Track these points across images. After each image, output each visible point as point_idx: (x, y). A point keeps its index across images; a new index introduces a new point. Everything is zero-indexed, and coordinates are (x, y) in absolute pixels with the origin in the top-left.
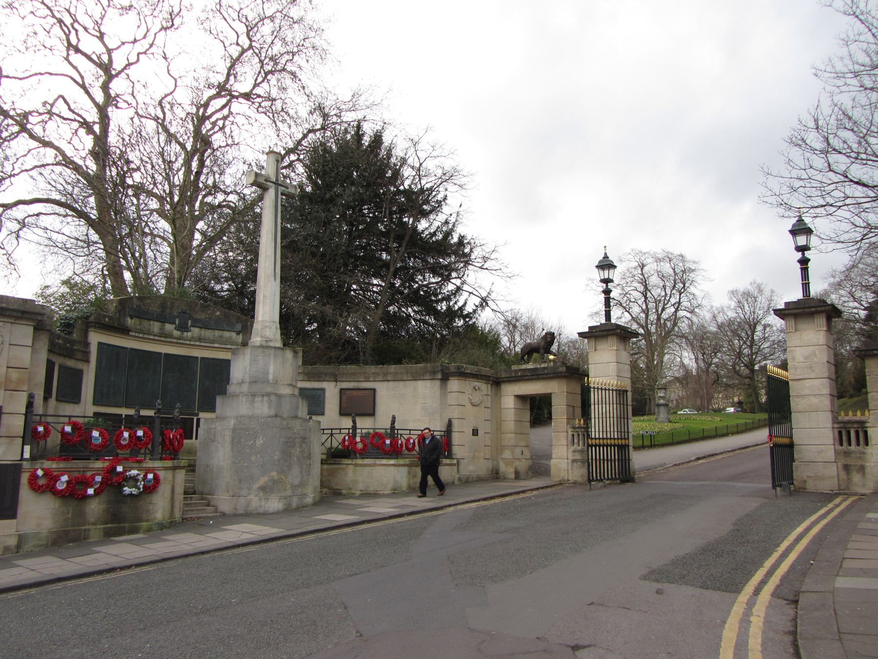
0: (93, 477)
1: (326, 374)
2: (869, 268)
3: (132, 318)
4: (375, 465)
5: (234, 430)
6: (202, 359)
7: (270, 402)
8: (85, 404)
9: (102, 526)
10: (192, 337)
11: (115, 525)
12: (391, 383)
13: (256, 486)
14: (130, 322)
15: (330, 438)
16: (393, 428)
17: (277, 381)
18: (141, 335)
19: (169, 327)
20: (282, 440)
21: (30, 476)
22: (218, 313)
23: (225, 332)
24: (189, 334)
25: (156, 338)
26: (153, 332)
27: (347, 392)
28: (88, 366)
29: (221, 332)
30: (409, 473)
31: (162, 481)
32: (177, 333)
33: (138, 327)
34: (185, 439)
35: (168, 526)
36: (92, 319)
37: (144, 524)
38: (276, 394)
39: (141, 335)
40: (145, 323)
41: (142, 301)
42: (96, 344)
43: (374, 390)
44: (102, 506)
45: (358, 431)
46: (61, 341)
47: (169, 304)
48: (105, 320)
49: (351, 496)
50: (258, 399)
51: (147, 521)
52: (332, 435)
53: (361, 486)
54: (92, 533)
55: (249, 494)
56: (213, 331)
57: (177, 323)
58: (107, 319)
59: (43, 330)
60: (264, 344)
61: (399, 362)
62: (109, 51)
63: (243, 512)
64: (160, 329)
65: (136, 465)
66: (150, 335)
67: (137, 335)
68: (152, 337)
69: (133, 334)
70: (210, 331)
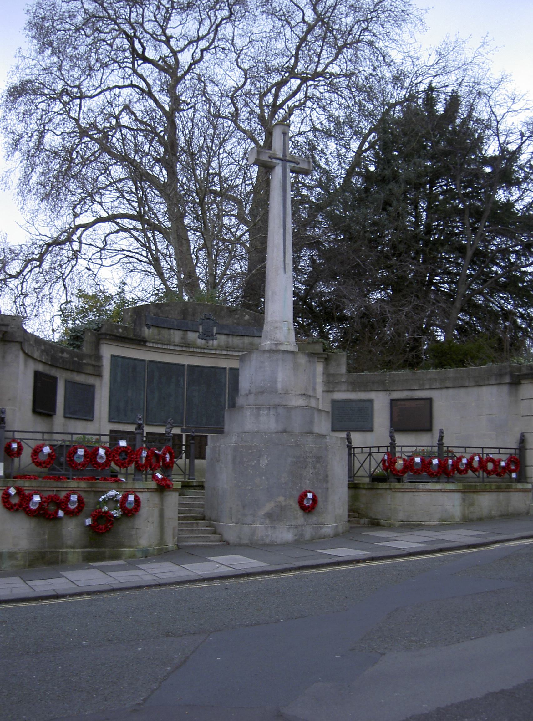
0: (68, 497)
1: (373, 382)
2: (370, 17)
3: (149, 328)
4: (418, 490)
5: (235, 449)
6: (189, 366)
7: (277, 415)
8: (100, 421)
9: (82, 550)
10: (219, 346)
11: (95, 550)
12: (451, 392)
13: (262, 512)
14: (147, 332)
15: (369, 457)
16: (440, 445)
17: (287, 390)
18: (159, 346)
19: (192, 336)
20: (290, 459)
21: (4, 494)
22: (247, 317)
23: (256, 338)
24: (215, 342)
25: (177, 348)
26: (174, 342)
27: (399, 403)
28: (101, 381)
29: (251, 339)
30: (464, 500)
31: (142, 505)
32: (201, 342)
33: (157, 337)
34: (197, 458)
35: (156, 553)
36: (103, 330)
37: (127, 551)
38: (284, 407)
39: (159, 346)
40: (165, 332)
41: (160, 309)
42: (109, 357)
43: (430, 400)
44: (79, 529)
45: (398, 449)
46: (65, 355)
47: (190, 310)
48: (118, 332)
49: (390, 527)
50: (264, 412)
51: (130, 547)
52: (370, 454)
53: (401, 516)
54: (70, 557)
55: (254, 522)
56: (242, 338)
57: (201, 330)
58: (120, 330)
59: (10, 342)
60: (273, 347)
61: (462, 363)
62: (175, 53)
63: (247, 542)
64: (182, 338)
65: (114, 485)
66: (170, 345)
67: (155, 345)
68: (172, 348)
69: (151, 345)
70: (238, 338)
